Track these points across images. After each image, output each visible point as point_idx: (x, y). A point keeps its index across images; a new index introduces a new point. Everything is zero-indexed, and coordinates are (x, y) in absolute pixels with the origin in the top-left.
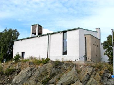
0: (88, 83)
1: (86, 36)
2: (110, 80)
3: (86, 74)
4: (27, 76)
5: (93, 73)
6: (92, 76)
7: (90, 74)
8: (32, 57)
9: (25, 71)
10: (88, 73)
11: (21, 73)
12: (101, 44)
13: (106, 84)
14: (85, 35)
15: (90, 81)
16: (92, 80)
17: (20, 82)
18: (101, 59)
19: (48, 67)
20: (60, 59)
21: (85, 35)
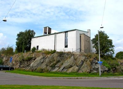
2: (97, 65)
3: (80, 61)
6: (85, 62)
7: (83, 61)
14: (80, 34)
15: (84, 65)
16: (85, 65)
20: (63, 51)
21: (80, 34)
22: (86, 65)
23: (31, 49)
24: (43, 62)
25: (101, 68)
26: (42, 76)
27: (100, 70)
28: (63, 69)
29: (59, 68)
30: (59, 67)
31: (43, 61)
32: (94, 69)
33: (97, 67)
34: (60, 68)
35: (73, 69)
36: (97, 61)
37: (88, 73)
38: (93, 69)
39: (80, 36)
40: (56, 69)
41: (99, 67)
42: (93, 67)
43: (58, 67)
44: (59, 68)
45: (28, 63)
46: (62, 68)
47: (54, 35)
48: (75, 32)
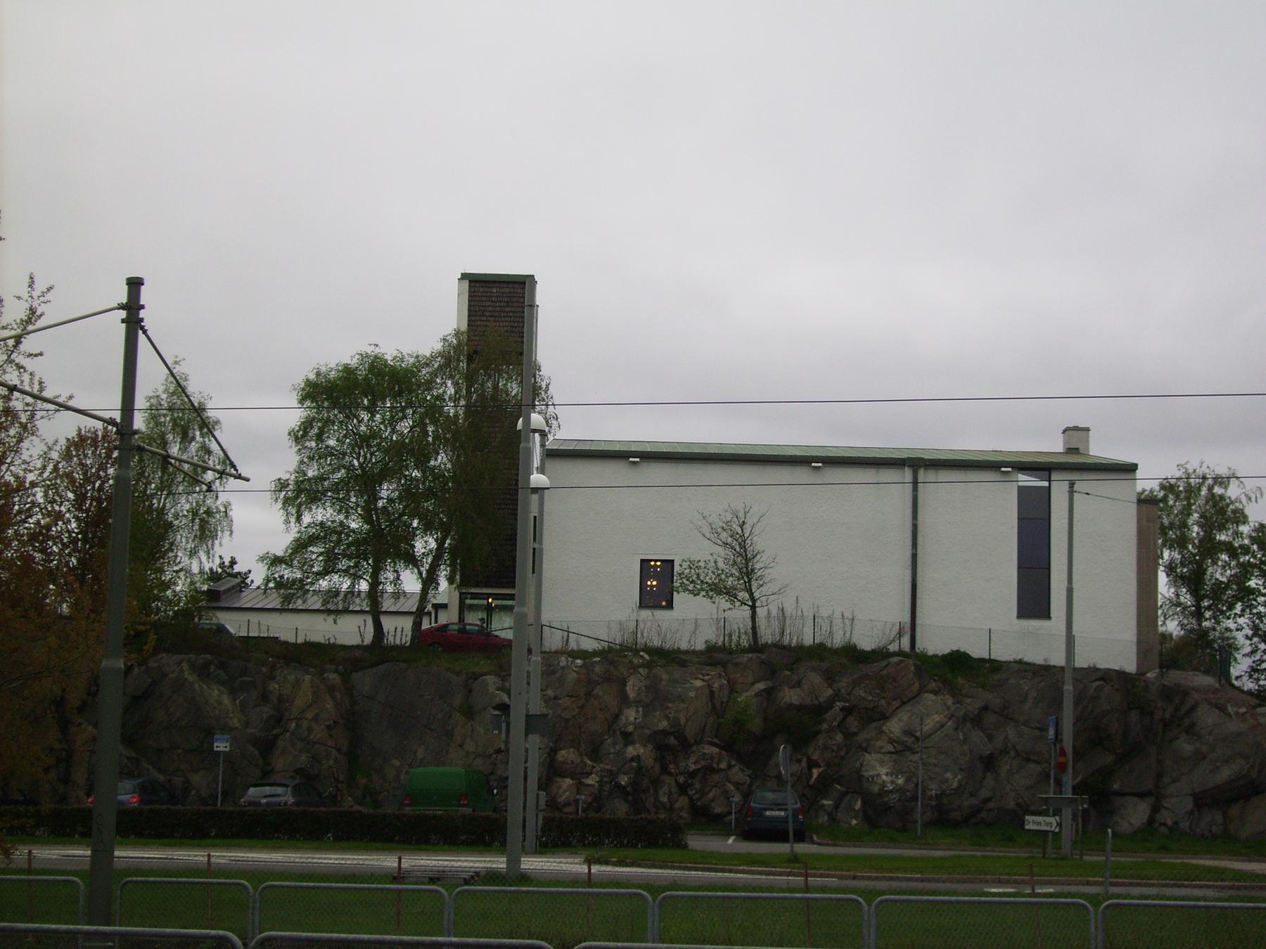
45: (812, 764)
47: (1076, 496)
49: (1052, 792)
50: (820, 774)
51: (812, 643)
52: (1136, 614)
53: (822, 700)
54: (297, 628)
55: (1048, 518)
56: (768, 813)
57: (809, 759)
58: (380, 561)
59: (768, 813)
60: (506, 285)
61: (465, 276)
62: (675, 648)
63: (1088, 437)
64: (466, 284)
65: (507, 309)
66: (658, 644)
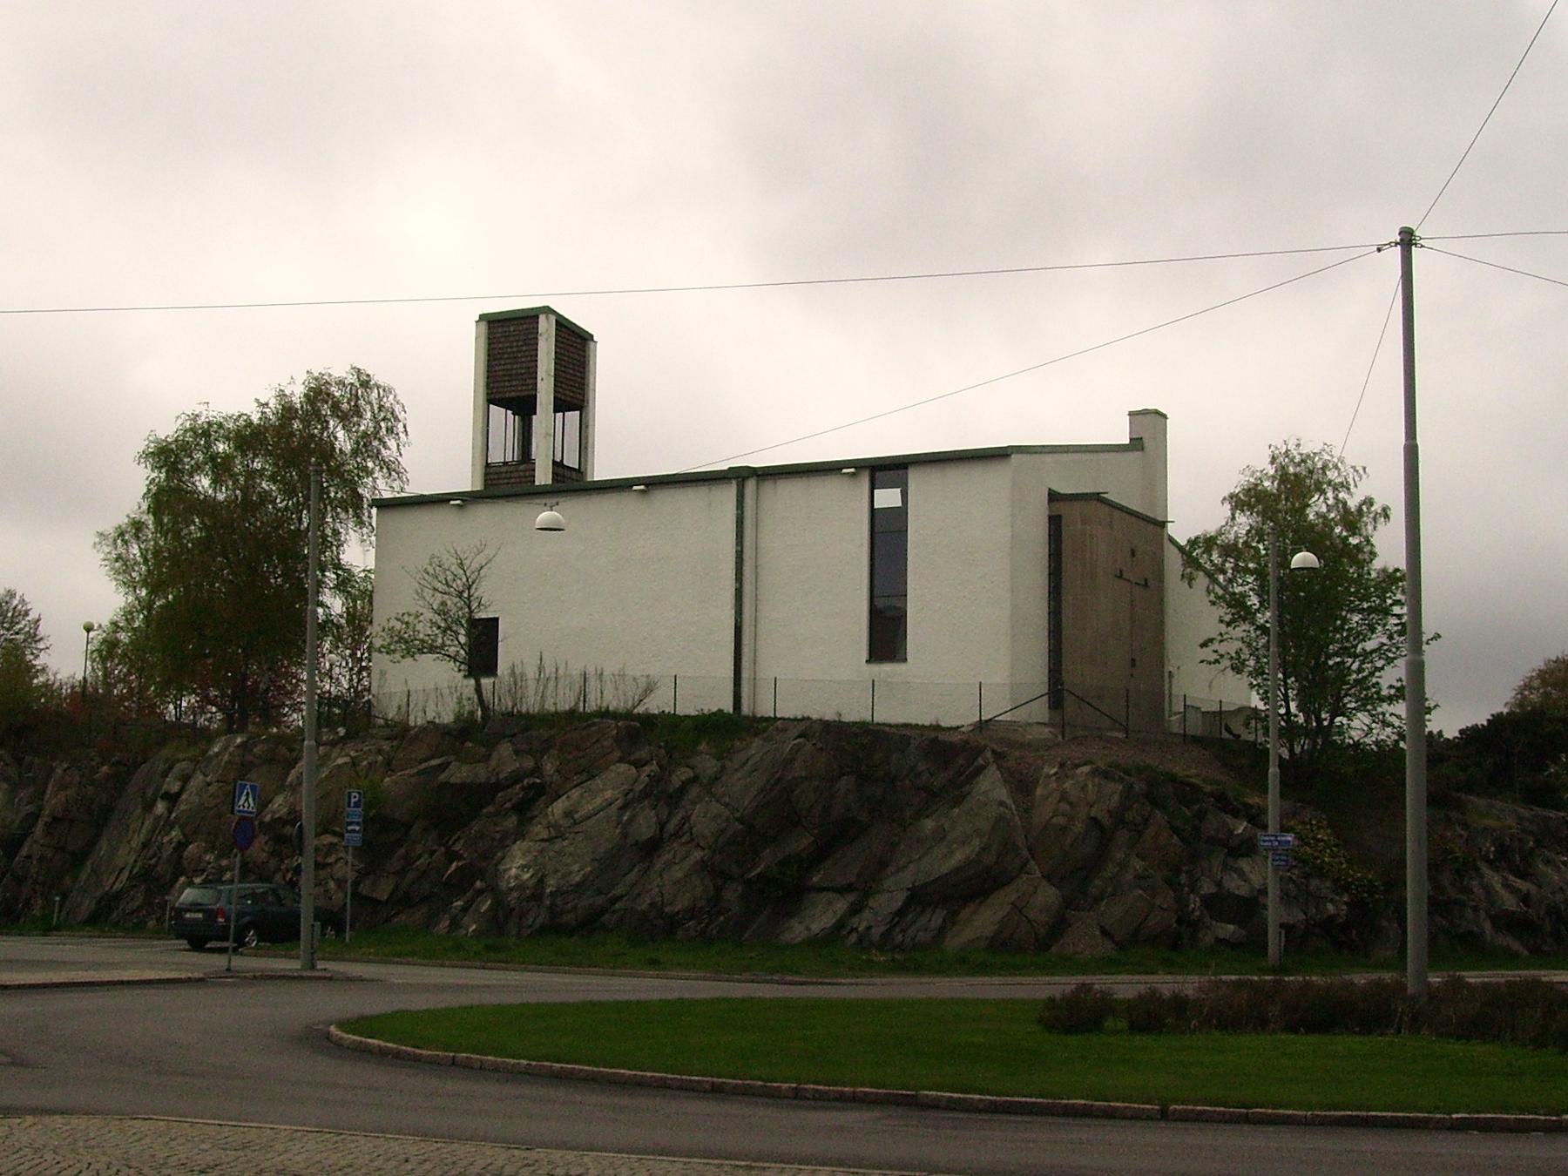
0: (1098, 882)
1: (1063, 508)
2: (1244, 864)
3: (1078, 827)
4: (625, 835)
5: (1129, 816)
6: (1123, 836)
7: (1106, 821)
8: (1428, 804)
9: (598, 801)
10: (1094, 819)
11: (568, 814)
12: (1173, 562)
13: (1214, 890)
14: (1053, 497)
15: (1110, 870)
16: (1123, 866)
17: (578, 885)
18: (1166, 675)
19: (1175, 837)
20: (854, 710)
21: (1053, 497)
22: (1138, 864)
23: (1458, 974)
24: (651, 848)
25: (1285, 897)
26: (796, 983)
27: (1274, 914)
28: (901, 913)
29: (851, 898)
30: (862, 891)
31: (662, 825)
32: (1220, 904)
33: (1244, 891)
34: (867, 894)
35: (1017, 908)
36: (1241, 827)
37: (1041, 911)
38: (1208, 902)
39: (1055, 522)
40: (821, 916)
41: (1263, 892)
42: (1207, 888)
43: (842, 891)
44: (855, 910)
45: (451, 856)
46: (887, 901)
47: (728, 494)
48: (996, 478)
49: (231, 940)
50: (458, 868)
51: (728, 707)
52: (1046, 679)
53: (501, 776)
54: (1221, 702)
55: (876, 537)
56: (188, 915)
57: (448, 849)
58: (1320, 649)
59: (188, 915)
60: (522, 322)
61: (482, 317)
62: (611, 708)
63: (1130, 433)
64: (484, 325)
65: (524, 348)
66: (625, 702)
